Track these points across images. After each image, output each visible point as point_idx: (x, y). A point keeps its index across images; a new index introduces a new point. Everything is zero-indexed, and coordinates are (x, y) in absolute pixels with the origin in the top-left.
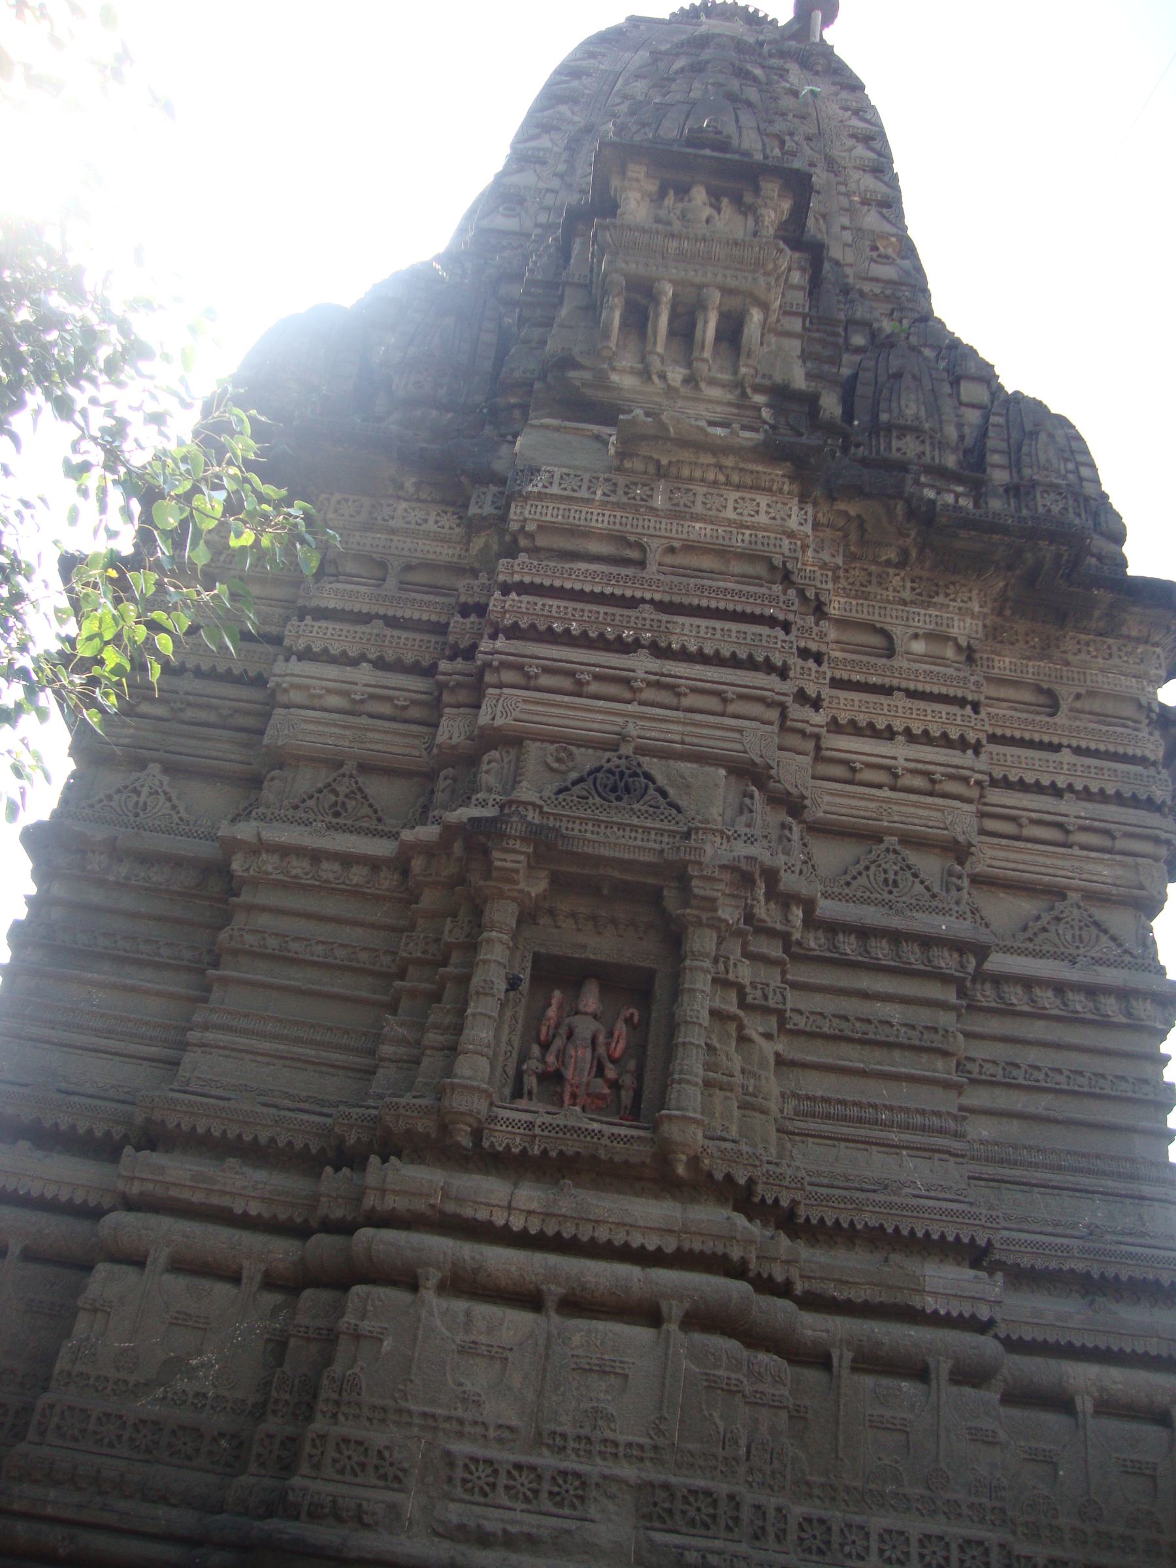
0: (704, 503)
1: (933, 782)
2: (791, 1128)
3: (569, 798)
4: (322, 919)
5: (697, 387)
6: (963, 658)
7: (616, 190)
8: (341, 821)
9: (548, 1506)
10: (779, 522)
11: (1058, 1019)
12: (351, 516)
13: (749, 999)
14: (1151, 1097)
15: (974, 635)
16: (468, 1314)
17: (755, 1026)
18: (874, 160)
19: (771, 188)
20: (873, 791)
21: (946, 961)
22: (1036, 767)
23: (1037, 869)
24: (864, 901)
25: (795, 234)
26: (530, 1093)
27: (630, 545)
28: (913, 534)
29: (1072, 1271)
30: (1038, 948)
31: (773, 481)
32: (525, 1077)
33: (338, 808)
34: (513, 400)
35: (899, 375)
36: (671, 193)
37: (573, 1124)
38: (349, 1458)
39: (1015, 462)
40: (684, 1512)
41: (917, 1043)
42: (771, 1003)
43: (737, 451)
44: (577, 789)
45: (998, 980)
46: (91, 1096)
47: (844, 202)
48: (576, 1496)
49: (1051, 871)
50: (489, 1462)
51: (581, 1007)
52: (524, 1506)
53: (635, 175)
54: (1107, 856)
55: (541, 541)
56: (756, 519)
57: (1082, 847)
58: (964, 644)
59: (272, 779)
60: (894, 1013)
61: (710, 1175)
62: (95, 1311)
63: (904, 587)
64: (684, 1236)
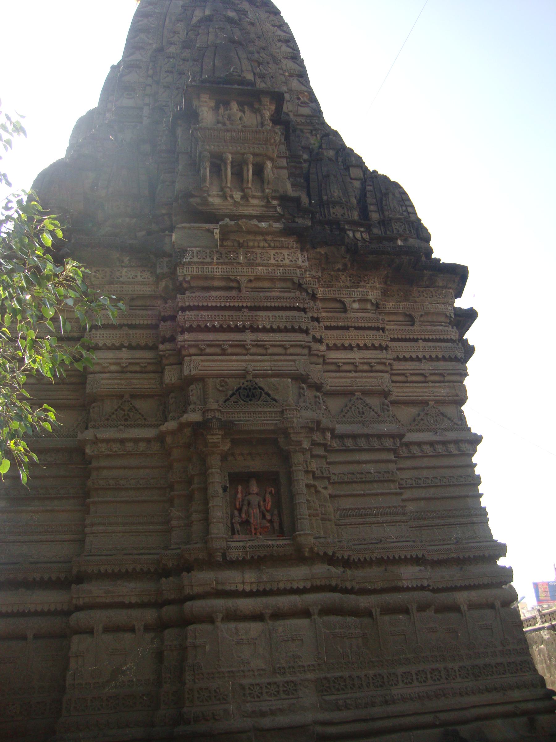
0: (261, 258)
1: (372, 367)
2: (340, 523)
3: (230, 403)
4: (130, 468)
5: (247, 200)
6: (375, 308)
7: (196, 106)
8: (129, 423)
9: (283, 696)
10: (294, 262)
11: (432, 456)
12: (103, 278)
13: (316, 475)
14: (472, 482)
15: (378, 298)
16: (236, 628)
17: (320, 485)
18: (292, 53)
19: (266, 100)
20: (348, 374)
21: (388, 443)
22: (410, 350)
23: (416, 394)
24: (353, 422)
25: (278, 119)
26: (238, 531)
27: (232, 281)
28: (348, 257)
29: (453, 558)
30: (421, 428)
31: (289, 244)
32: (235, 525)
33: (126, 417)
34: (164, 212)
35: (328, 176)
36: (221, 106)
37: (262, 543)
38: (204, 695)
39: (381, 209)
40: (334, 686)
41: (382, 479)
42: (325, 475)
43: (273, 233)
44: (234, 398)
45: (408, 445)
46: (45, 563)
47: (283, 79)
48: (293, 690)
49: (421, 394)
50: (258, 684)
51: (251, 491)
52: (275, 698)
53: (205, 100)
54: (442, 384)
55: (193, 284)
56: (284, 262)
57: (432, 382)
58: (374, 302)
59: (94, 408)
60: (371, 468)
61: (318, 554)
62: (77, 656)
63: (347, 280)
64: (313, 580)
